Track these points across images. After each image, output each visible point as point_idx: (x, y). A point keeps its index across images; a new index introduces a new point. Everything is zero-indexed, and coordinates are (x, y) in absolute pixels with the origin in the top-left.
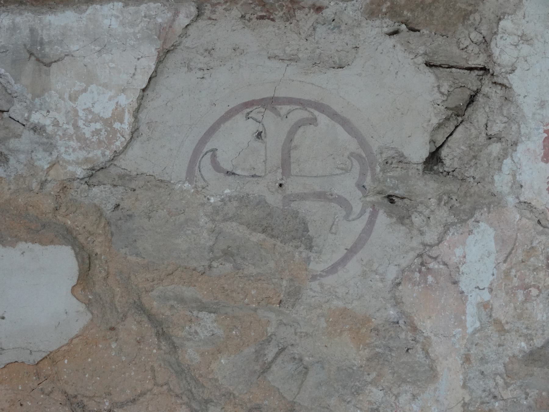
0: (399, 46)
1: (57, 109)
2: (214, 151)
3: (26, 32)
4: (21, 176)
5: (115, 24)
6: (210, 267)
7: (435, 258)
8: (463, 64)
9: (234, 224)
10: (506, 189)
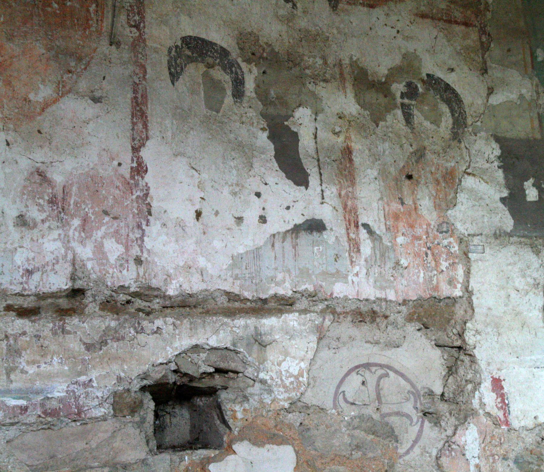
0: (423, 336)
1: (272, 371)
2: (344, 392)
3: (252, 329)
4: (257, 408)
5: (296, 324)
6: (351, 454)
7: (454, 443)
8: (451, 345)
9: (358, 431)
10: (478, 407)
